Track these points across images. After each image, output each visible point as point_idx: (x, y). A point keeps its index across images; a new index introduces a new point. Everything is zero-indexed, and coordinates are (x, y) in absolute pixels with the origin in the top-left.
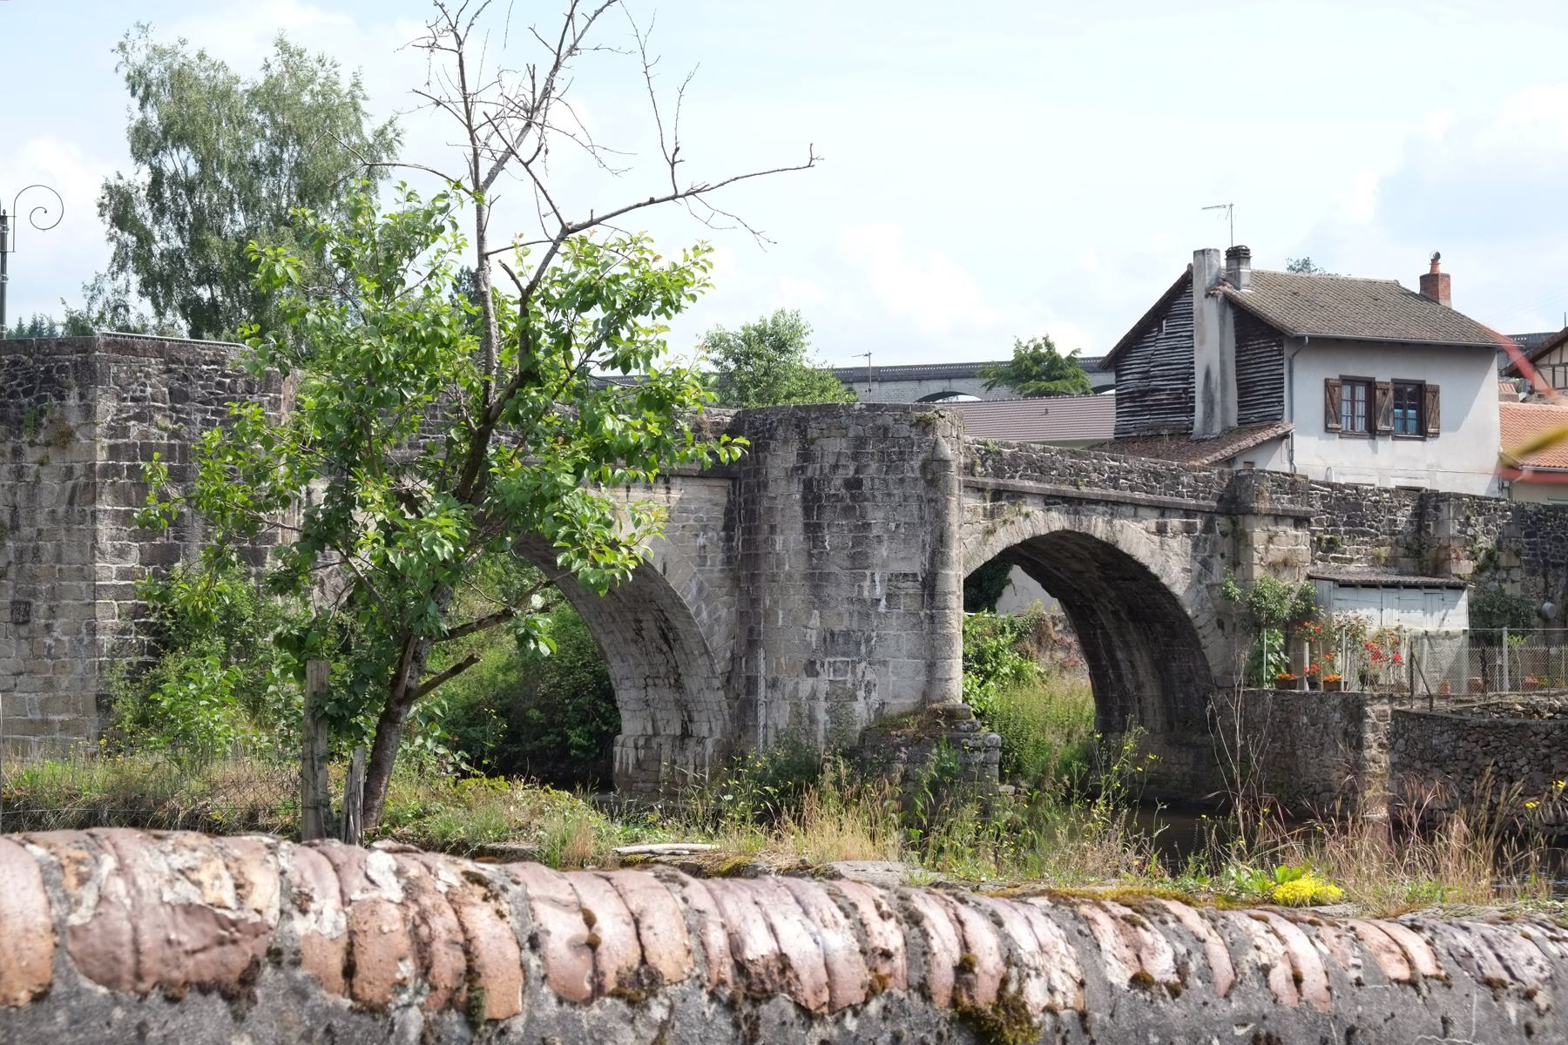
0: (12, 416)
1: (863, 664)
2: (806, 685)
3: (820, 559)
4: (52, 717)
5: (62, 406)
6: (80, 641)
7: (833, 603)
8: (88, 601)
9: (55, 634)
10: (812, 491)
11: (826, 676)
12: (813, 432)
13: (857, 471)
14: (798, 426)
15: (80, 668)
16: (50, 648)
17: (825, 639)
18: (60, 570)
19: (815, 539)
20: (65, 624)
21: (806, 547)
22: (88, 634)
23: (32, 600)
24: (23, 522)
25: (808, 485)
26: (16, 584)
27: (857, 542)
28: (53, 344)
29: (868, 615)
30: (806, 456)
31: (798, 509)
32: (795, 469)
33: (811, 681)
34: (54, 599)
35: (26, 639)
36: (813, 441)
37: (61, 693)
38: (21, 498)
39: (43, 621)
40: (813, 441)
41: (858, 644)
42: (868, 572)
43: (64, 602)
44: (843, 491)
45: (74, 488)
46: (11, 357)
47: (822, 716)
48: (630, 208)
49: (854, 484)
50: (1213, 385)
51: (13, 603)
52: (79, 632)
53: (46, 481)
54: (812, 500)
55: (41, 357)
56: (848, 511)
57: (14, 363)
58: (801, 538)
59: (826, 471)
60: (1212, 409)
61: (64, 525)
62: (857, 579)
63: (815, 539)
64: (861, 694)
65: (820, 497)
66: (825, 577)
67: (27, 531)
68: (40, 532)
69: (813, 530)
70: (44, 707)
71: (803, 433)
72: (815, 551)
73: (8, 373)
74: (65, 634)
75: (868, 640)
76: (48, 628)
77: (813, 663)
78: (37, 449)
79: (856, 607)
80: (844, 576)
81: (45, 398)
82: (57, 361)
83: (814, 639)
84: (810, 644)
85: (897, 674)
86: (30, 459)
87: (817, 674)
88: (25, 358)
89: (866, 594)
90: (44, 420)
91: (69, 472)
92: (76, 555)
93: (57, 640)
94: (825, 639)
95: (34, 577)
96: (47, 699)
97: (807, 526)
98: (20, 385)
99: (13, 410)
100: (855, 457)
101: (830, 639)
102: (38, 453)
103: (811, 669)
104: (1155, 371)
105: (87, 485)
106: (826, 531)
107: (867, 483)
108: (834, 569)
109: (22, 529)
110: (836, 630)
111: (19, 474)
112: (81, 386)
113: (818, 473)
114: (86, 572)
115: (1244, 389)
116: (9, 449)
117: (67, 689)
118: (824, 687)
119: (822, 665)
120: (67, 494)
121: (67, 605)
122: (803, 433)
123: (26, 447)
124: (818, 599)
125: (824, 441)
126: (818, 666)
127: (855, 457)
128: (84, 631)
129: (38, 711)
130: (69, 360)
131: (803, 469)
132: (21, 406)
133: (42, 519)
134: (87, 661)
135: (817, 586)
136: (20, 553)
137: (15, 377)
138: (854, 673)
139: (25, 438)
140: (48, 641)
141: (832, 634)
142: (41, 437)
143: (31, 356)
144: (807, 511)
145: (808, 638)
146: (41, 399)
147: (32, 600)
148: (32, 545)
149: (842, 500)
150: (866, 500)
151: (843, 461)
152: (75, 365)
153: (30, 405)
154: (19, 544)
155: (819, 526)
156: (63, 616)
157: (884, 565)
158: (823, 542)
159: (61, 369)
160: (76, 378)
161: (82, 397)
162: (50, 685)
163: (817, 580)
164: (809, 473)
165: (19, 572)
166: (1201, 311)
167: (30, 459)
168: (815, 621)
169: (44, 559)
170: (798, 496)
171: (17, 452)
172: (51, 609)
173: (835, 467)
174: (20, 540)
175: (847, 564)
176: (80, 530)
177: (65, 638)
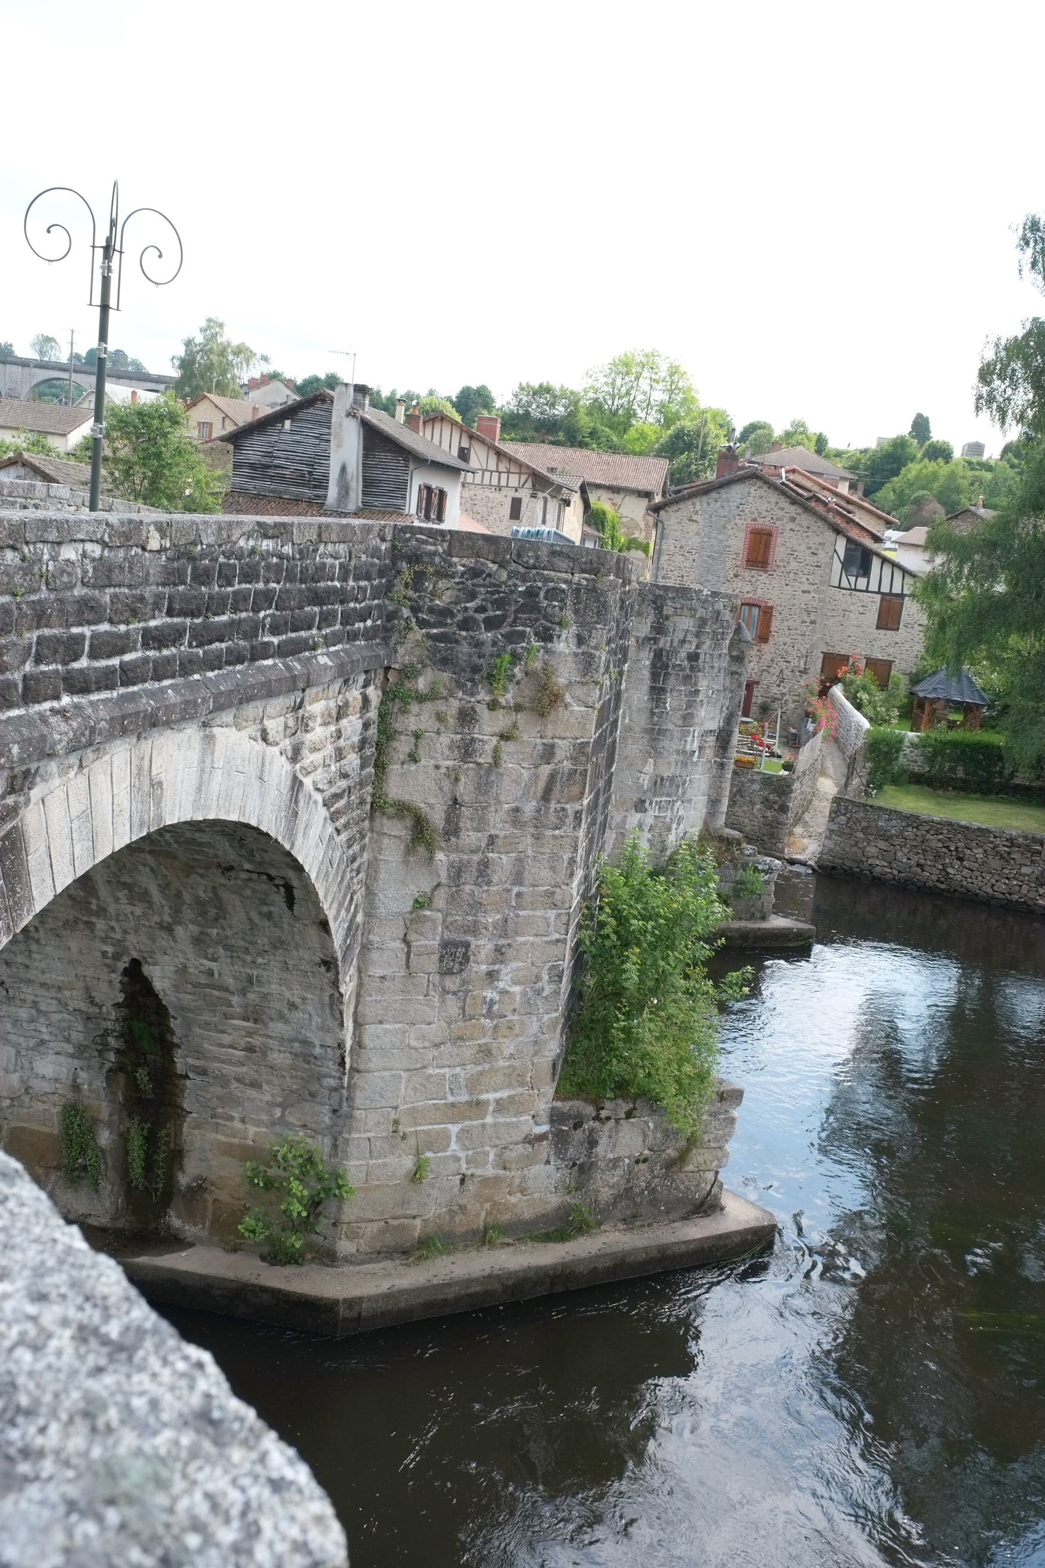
0: (463, 658)
1: (679, 802)
2: (635, 818)
3: (660, 717)
4: (484, 1097)
5: (547, 651)
6: (539, 992)
7: (666, 754)
8: (557, 936)
9: (501, 985)
10: (661, 659)
11: (652, 812)
12: (668, 610)
13: (697, 647)
14: (654, 602)
15: (534, 1028)
16: (492, 1003)
17: (656, 783)
18: (519, 895)
19: (658, 700)
20: (518, 969)
21: (649, 706)
22: (550, 982)
23: (470, 938)
24: (465, 823)
25: (658, 654)
26: (446, 915)
27: (689, 705)
28: (544, 553)
29: (686, 764)
30: (659, 629)
31: (646, 674)
32: (648, 639)
33: (639, 815)
34: (505, 935)
35: (455, 993)
36: (667, 618)
37: (502, 1063)
38: (465, 789)
39: (484, 968)
40: (667, 618)
41: (678, 787)
42: (692, 729)
43: (520, 939)
44: (686, 662)
45: (552, 777)
46: (470, 562)
47: (644, 846)
48: (106, 281)
49: (693, 657)
50: (349, 477)
51: (445, 945)
52: (538, 978)
53: (509, 764)
54: (660, 668)
55: (522, 570)
56: (687, 679)
57: (474, 573)
58: (646, 698)
59: (675, 644)
60: (347, 493)
61: (532, 830)
62: (684, 734)
63: (658, 700)
64: (674, 826)
65: (667, 666)
66: (661, 732)
67: (470, 837)
68: (492, 840)
69: (657, 692)
70: (474, 1084)
71: (659, 609)
72: (657, 711)
73: (461, 585)
74: (515, 983)
75: (684, 784)
76: (492, 976)
77: (643, 802)
78: (500, 713)
79: (681, 758)
80: (676, 732)
81: (522, 635)
82: (546, 580)
83: (646, 782)
84: (642, 786)
85: (695, 809)
86: (487, 729)
87: (646, 810)
88: (495, 567)
89: (688, 747)
90: (516, 670)
91: (548, 753)
92: (545, 873)
93: (504, 992)
94: (656, 783)
95: (477, 906)
96: (481, 1073)
97: (652, 688)
98: (481, 609)
99: (465, 648)
100: (698, 635)
101: (659, 782)
102: (501, 721)
103: (640, 806)
104: (276, 454)
105: (572, 773)
106: (668, 695)
107: (702, 657)
108: (671, 726)
109: (463, 834)
110: (665, 776)
111: (466, 750)
112: (582, 625)
113: (668, 645)
114: (558, 897)
115: (369, 484)
116: (454, 711)
117: (512, 1056)
118: (649, 820)
119: (651, 804)
120: (542, 784)
121: (524, 944)
122: (659, 609)
123: (482, 710)
124: (654, 750)
125: (677, 619)
126: (647, 804)
127: (698, 635)
128: (546, 977)
129: (464, 1090)
130: (566, 582)
131: (656, 640)
132: (478, 644)
133: (498, 823)
134: (546, 1017)
135: (655, 739)
136: (457, 872)
137: (472, 596)
138: (672, 809)
139: (483, 695)
140: (489, 994)
141: (662, 779)
142: (508, 698)
143: (502, 565)
144: (655, 676)
145: (641, 781)
146: (514, 637)
147: (470, 938)
148: (476, 858)
149: (683, 670)
150: (699, 671)
151: (689, 638)
152: (577, 591)
153: (494, 644)
154: (454, 857)
155: (663, 690)
156: (517, 958)
157: (701, 725)
158: (665, 703)
159: (553, 594)
160: (576, 612)
161: (580, 640)
162: (486, 1053)
163: (655, 734)
164: (661, 644)
165: (453, 899)
166: (340, 425)
167: (487, 729)
168: (649, 768)
169: (495, 879)
170: (647, 663)
171: (467, 717)
172: (498, 950)
173: (683, 642)
174: (457, 850)
175: (680, 723)
176: (555, 837)
177: (516, 989)
